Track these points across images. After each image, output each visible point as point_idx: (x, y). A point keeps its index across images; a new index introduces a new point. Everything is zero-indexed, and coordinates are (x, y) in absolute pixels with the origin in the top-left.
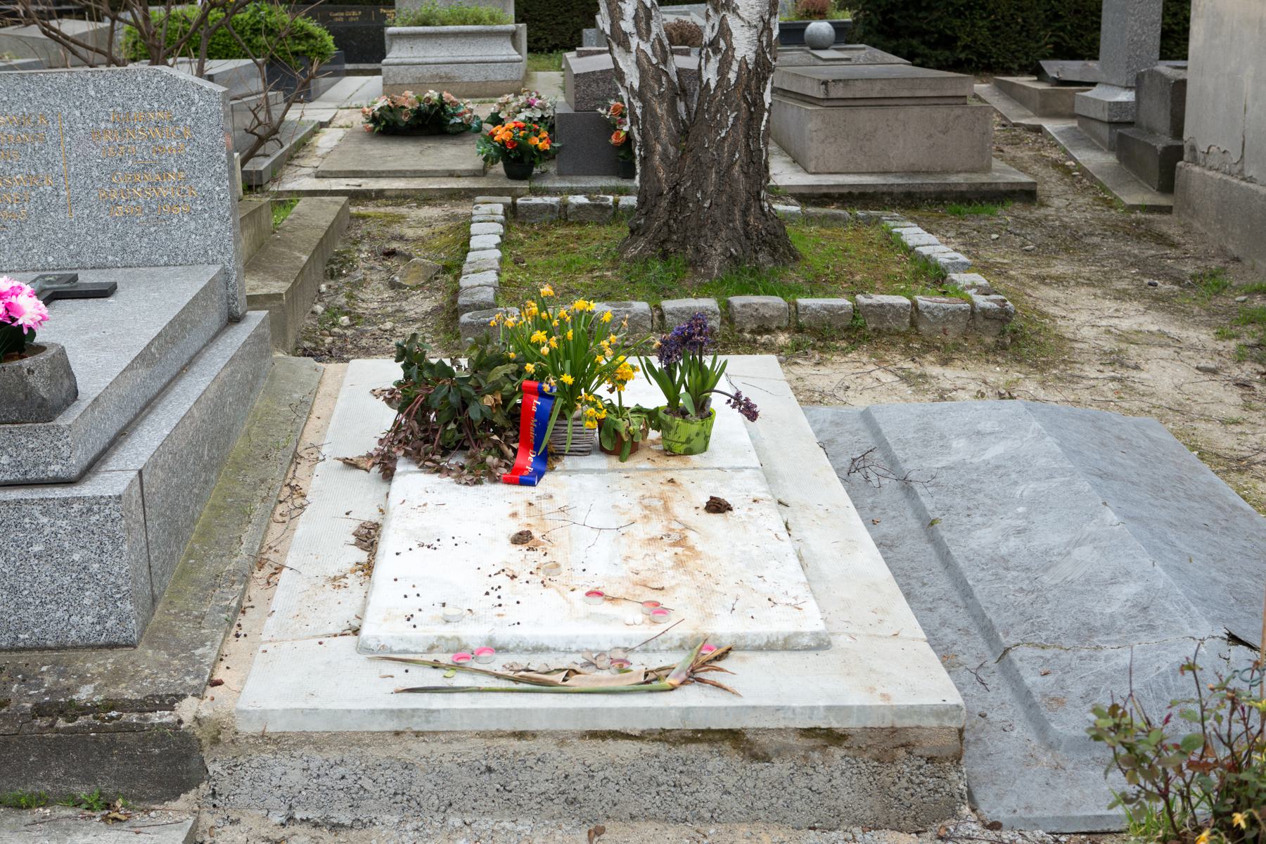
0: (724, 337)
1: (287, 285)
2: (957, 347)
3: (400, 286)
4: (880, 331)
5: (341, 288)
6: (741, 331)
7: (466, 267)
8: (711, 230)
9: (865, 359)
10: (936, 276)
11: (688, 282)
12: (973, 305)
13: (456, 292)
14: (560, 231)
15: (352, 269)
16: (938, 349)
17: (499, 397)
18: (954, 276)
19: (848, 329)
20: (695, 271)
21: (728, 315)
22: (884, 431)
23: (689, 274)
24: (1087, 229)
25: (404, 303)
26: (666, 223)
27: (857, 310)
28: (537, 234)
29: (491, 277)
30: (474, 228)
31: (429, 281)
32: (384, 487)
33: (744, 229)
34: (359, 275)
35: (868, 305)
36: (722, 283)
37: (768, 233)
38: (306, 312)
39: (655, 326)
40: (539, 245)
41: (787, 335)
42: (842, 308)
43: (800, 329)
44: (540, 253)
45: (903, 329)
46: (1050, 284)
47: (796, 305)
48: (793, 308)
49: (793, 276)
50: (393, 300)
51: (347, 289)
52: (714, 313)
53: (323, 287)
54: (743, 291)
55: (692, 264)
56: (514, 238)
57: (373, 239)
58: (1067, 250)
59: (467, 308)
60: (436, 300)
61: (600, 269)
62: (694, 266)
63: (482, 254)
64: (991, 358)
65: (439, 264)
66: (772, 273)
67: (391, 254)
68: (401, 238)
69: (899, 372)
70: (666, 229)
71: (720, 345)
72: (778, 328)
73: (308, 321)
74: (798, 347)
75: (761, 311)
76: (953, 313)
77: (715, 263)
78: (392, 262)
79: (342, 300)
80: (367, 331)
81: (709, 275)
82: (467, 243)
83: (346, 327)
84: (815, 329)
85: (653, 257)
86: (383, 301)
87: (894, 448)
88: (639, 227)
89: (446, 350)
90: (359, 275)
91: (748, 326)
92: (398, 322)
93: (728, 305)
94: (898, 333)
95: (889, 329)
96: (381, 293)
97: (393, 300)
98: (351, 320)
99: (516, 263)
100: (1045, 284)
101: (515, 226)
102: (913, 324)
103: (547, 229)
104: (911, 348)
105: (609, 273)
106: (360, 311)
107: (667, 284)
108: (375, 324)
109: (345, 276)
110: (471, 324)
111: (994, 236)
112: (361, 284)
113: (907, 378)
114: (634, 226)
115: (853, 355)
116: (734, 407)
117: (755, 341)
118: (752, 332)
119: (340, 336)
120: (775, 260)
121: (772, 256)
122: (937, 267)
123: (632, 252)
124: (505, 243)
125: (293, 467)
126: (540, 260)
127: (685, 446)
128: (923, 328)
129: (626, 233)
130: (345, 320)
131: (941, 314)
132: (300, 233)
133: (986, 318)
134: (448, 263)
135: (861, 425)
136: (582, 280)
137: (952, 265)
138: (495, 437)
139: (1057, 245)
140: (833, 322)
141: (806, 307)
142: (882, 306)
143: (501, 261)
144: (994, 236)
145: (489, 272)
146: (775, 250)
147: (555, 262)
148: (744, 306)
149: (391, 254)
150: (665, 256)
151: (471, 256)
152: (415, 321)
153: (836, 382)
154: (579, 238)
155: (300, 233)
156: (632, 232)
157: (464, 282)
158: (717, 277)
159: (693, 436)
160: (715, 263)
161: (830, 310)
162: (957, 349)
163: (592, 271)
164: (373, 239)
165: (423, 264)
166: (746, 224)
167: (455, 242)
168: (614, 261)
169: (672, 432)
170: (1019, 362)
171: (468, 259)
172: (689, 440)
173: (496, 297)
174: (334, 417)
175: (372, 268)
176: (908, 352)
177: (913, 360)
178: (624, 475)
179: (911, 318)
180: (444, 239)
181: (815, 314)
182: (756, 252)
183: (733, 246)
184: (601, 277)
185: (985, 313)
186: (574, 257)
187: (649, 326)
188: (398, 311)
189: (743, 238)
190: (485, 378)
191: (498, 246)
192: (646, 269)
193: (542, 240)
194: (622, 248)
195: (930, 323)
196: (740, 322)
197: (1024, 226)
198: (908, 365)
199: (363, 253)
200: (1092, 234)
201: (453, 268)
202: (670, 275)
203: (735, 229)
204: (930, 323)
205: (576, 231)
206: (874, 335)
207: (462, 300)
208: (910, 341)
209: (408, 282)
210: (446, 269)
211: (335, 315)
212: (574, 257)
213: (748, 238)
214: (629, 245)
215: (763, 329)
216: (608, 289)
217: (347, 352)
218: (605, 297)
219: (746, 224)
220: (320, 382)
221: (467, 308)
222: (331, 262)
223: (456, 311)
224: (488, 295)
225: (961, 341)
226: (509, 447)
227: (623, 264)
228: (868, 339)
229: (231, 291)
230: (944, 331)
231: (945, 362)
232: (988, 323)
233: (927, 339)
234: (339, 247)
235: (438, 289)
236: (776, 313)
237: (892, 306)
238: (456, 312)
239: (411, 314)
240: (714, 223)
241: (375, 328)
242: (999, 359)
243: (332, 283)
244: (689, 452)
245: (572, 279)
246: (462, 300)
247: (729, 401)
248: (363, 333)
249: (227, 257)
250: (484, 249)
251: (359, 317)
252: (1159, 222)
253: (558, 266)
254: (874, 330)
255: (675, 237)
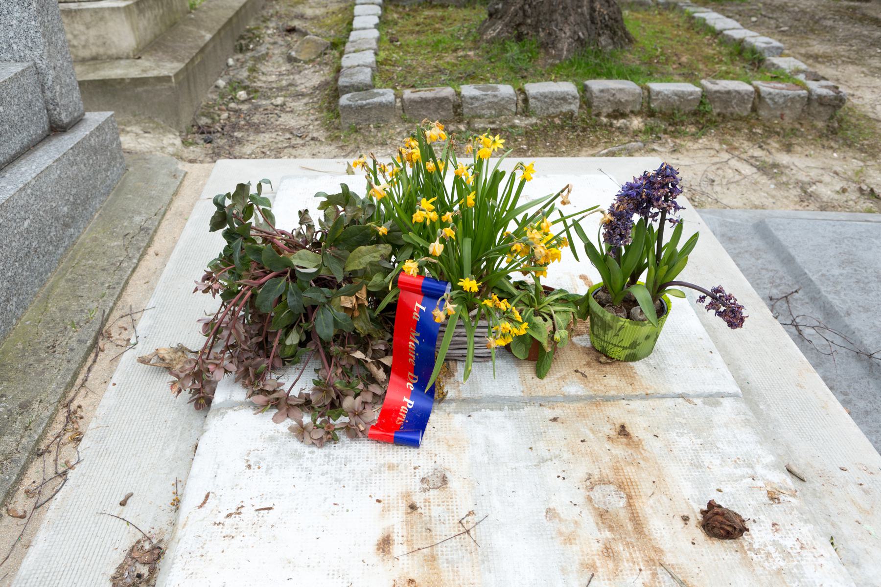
0: (583, 120)
1: (178, 66)
2: (794, 132)
3: (296, 60)
4: (724, 117)
5: (246, 61)
6: (598, 115)
7: (348, 47)
8: (562, 15)
9: (717, 146)
10: (754, 61)
11: (541, 62)
12: (810, 92)
13: (339, 70)
14: (427, 13)
15: (258, 44)
16: (778, 134)
17: (362, 294)
18: (776, 60)
19: (695, 113)
20: (547, 53)
21: (586, 98)
22: (798, 260)
23: (542, 55)
24: (822, 14)
25: (297, 77)
26: (522, 8)
27: (706, 96)
28: (409, 15)
29: (369, 57)
30: (358, 10)
31: (319, 56)
32: (195, 418)
33: (591, 15)
34: (263, 50)
35: (716, 92)
36: (572, 64)
37: (610, 18)
38: (208, 87)
39: (520, 110)
40: (408, 24)
41: (640, 120)
42: (691, 94)
43: (651, 114)
44: (412, 32)
45: (745, 114)
46: (823, 63)
47: (649, 90)
48: (646, 94)
49: (631, 58)
50: (289, 73)
51: (250, 64)
52: (574, 97)
53: (231, 62)
54: (597, 75)
55: (544, 46)
56: (390, 18)
57: (280, 17)
58: (812, 31)
59: (347, 89)
60: (324, 75)
61: (464, 49)
62: (545, 48)
63: (363, 34)
64: (826, 143)
65: (328, 41)
66: (612, 54)
67: (291, 30)
68: (302, 17)
69: (753, 161)
70: (521, 13)
71: (580, 129)
72: (632, 112)
73: (210, 96)
74: (650, 130)
75: (618, 96)
76: (793, 100)
77: (564, 45)
78: (293, 38)
79: (244, 74)
80: (260, 106)
81: (559, 57)
82: (350, 23)
83: (243, 102)
84: (664, 114)
85: (509, 38)
86: (281, 74)
87: (823, 289)
88: (497, 11)
89: (328, 130)
90: (263, 50)
91: (605, 110)
92: (290, 96)
93: (585, 89)
94: (741, 118)
95: (732, 114)
96: (279, 66)
97: (289, 73)
98: (248, 94)
99: (391, 41)
100: (819, 62)
101: (391, 7)
102: (754, 109)
103: (416, 11)
104: (755, 134)
105: (471, 53)
106: (259, 84)
107: (523, 65)
108: (269, 98)
109: (252, 50)
110: (350, 106)
111: (754, 19)
112: (264, 57)
113: (764, 169)
114: (493, 10)
115: (703, 141)
116: (709, 307)
117: (611, 125)
118: (608, 116)
119: (236, 111)
120: (614, 43)
121: (612, 39)
122: (753, 51)
123: (491, 34)
124: (383, 22)
125: (93, 355)
126: (411, 39)
127: (627, 352)
128: (763, 113)
129: (484, 16)
130: (242, 94)
131: (781, 101)
132: (213, 13)
133: (821, 104)
134: (336, 41)
135: (757, 242)
136: (448, 59)
137: (768, 49)
138: (359, 355)
139: (805, 27)
140: (682, 107)
141: (658, 93)
142: (729, 92)
143: (379, 40)
144: (754, 19)
145: (367, 52)
146: (615, 33)
147: (425, 42)
148: (602, 91)
149: (291, 30)
150: (519, 38)
151: (353, 36)
152: (303, 95)
153: (700, 174)
154: (442, 19)
155: (213, 13)
156: (491, 15)
157: (346, 62)
158: (567, 58)
159: (641, 340)
160: (564, 45)
161: (681, 96)
162: (795, 134)
163: (455, 50)
164: (280, 17)
165: (314, 41)
166: (593, 9)
167: (343, 21)
168: (475, 41)
169: (611, 333)
170: (850, 146)
171: (351, 38)
172: (634, 345)
173: (373, 78)
174: (174, 256)
175: (275, 43)
176: (751, 137)
177: (760, 147)
178: (549, 413)
179: (753, 103)
180: (335, 18)
181: (666, 99)
182: (599, 35)
183: (581, 29)
184: (465, 56)
185: (822, 100)
186: (439, 37)
187: (514, 110)
188: (290, 85)
189: (589, 23)
190: (341, 260)
191: (377, 26)
192: (504, 50)
193: (412, 19)
194: (482, 31)
195: (770, 109)
196: (597, 107)
197: (773, 11)
198: (758, 153)
199: (270, 30)
200: (825, 18)
201: (338, 45)
202: (525, 56)
203: (582, 14)
204: (770, 109)
205: (440, 13)
206: (719, 119)
207: (343, 81)
208: (752, 126)
209: (302, 57)
210: (334, 46)
211: (235, 89)
212: (439, 37)
213: (593, 22)
214: (488, 27)
215: (618, 114)
216: (471, 68)
217: (240, 129)
218: (471, 78)
219: (593, 9)
220: (176, 193)
221: (347, 89)
222: (242, 37)
223: (336, 89)
224: (365, 76)
225: (798, 126)
226: (379, 364)
227: (484, 45)
228: (713, 123)
229: (49, 94)
230: (782, 117)
231: (788, 148)
232: (821, 109)
233: (768, 124)
234: (252, 24)
235: (326, 64)
236: (631, 98)
237: (738, 92)
238: (337, 92)
239: (301, 88)
240: (564, 8)
241: (268, 102)
242: (833, 144)
243: (240, 56)
244: (633, 358)
245: (440, 58)
246: (343, 81)
247: (702, 299)
248: (257, 107)
249: (37, 52)
250: (364, 29)
251: (256, 91)
252: (867, 8)
253: (427, 45)
254: (719, 114)
255: (529, 21)
